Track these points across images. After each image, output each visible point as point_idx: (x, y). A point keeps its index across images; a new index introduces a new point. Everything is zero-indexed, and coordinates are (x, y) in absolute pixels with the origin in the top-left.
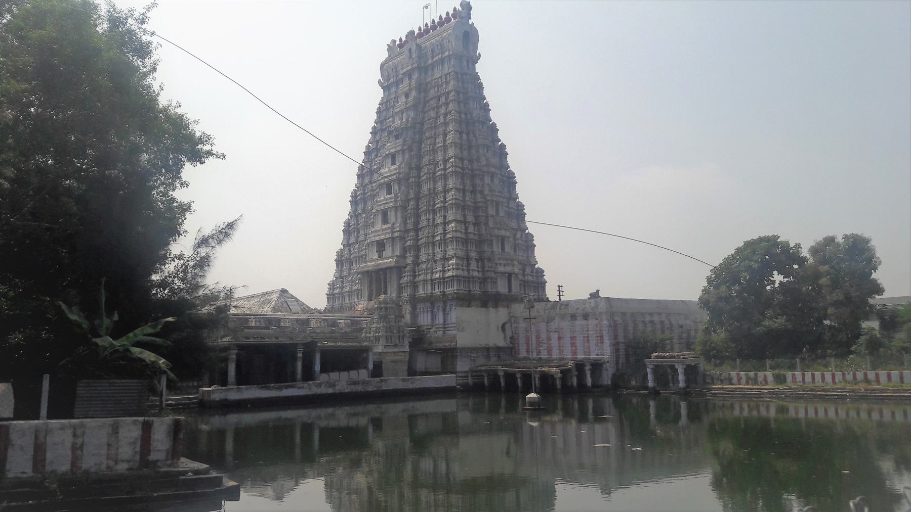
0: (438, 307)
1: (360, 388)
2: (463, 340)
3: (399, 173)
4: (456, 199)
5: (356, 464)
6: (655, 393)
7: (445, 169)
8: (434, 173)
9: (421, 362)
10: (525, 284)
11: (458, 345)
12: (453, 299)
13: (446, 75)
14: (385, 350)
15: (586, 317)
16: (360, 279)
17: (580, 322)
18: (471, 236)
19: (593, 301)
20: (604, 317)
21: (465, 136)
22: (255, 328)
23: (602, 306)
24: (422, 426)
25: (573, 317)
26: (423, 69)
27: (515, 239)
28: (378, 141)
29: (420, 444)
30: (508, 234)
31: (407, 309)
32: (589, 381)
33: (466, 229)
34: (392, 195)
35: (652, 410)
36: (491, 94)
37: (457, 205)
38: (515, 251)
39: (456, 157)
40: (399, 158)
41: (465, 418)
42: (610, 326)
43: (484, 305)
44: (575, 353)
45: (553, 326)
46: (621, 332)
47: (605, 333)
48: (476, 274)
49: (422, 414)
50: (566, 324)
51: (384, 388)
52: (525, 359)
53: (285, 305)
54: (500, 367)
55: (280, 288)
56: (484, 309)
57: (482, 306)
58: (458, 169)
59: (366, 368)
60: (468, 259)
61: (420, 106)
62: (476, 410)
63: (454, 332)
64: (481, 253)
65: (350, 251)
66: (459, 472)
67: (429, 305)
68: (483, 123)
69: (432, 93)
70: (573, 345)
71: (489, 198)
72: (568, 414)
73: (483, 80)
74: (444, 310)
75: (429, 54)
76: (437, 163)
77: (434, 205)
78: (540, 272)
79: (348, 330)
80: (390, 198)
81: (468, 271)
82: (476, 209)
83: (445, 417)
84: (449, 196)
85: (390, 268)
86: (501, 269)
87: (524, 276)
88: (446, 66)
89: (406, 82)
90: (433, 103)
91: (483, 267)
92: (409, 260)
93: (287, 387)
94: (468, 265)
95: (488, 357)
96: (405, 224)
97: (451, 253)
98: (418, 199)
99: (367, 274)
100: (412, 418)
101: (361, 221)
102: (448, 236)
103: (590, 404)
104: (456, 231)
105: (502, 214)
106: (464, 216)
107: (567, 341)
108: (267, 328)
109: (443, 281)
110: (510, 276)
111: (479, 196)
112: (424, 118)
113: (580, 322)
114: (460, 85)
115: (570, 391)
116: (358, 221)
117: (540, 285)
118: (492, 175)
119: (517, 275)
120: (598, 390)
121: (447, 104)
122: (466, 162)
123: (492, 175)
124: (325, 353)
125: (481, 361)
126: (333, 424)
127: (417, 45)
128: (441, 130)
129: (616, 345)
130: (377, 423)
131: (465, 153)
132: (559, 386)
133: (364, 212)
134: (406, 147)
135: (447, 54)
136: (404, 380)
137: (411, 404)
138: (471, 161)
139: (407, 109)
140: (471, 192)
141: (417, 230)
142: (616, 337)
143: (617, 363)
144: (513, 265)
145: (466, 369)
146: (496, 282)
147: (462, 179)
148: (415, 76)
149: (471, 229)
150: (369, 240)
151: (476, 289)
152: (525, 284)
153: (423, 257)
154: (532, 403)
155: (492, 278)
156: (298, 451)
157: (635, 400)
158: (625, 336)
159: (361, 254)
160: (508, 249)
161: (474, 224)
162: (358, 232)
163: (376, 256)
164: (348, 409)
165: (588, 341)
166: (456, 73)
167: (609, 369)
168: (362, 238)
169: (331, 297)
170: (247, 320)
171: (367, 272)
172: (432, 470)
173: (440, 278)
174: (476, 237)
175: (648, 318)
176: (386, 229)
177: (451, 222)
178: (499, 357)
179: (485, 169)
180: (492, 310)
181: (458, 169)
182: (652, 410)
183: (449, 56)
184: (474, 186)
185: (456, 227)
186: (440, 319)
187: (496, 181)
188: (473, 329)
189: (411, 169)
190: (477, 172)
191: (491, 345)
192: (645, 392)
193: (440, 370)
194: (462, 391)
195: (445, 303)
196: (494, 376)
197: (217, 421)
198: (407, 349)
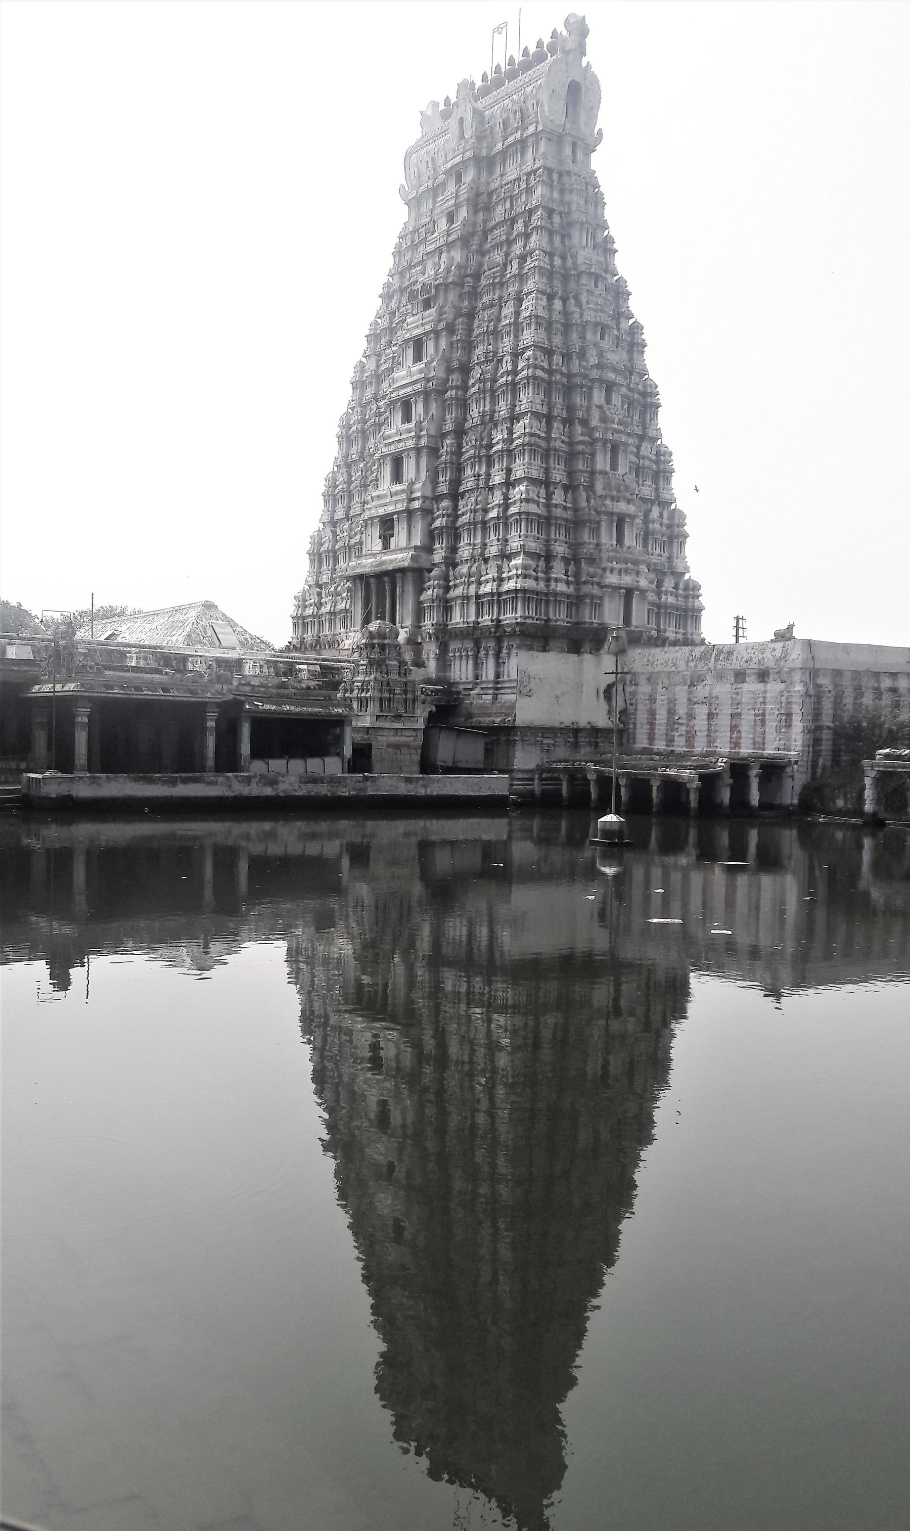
0: (487, 650)
1: (324, 790)
2: (528, 712)
3: (428, 380)
4: (532, 435)
5: (324, 923)
6: (875, 823)
7: (515, 372)
8: (494, 380)
9: (446, 748)
10: (658, 610)
11: (518, 723)
12: (513, 635)
13: (528, 174)
14: (378, 724)
15: (763, 676)
16: (349, 590)
17: (751, 686)
18: (558, 512)
19: (779, 645)
20: (797, 677)
21: (558, 304)
22: (135, 669)
23: (796, 656)
24: (443, 861)
25: (740, 676)
26: (486, 162)
27: (646, 521)
28: (393, 314)
29: (443, 894)
30: (632, 509)
31: (430, 650)
32: (755, 797)
33: (549, 496)
34: (414, 422)
35: (867, 856)
36: (619, 218)
37: (532, 448)
38: (645, 545)
39: (536, 346)
40: (429, 348)
41: (523, 851)
42: (807, 695)
43: (575, 648)
44: (736, 744)
45: (701, 691)
46: (827, 706)
47: (796, 709)
48: (562, 587)
49: (444, 843)
50: (723, 690)
51: (370, 792)
52: (645, 751)
53: (210, 632)
54: (591, 766)
55: (201, 598)
56: (573, 658)
57: (570, 651)
58: (539, 373)
59: (339, 754)
60: (548, 557)
61: (474, 239)
62: (544, 841)
63: (513, 697)
64: (575, 546)
65: (334, 533)
66: (513, 946)
67: (470, 645)
68: (597, 278)
69: (499, 213)
70: (734, 728)
71: (597, 435)
72: (707, 853)
73: (605, 187)
74: (497, 656)
75: (498, 130)
76: (500, 361)
77: (490, 446)
78: (692, 590)
79: (313, 684)
80: (409, 431)
81: (548, 580)
82: (571, 456)
83: (488, 850)
84: (519, 428)
85: (402, 570)
86: (612, 579)
87: (659, 594)
88: (529, 154)
89: (451, 188)
90: (500, 234)
91: (577, 575)
92: (438, 556)
93: (185, 781)
94: (548, 569)
95: (576, 745)
96: (434, 483)
97: (515, 544)
98: (460, 432)
99: (361, 578)
100: (425, 847)
101: (357, 475)
102: (513, 510)
103: (754, 837)
104: (527, 500)
105: (622, 469)
106: (547, 471)
107: (723, 722)
108: (158, 671)
109: (498, 599)
110: (629, 593)
111: (579, 429)
112: (481, 265)
113: (751, 686)
114: (556, 195)
115: (716, 813)
116: (350, 476)
117: (688, 613)
118: (609, 388)
119: (643, 592)
120: (773, 813)
121: (527, 236)
122: (557, 359)
123: (609, 388)
124: (261, 723)
125: (561, 752)
126: (275, 849)
127: (475, 111)
128: (512, 289)
129: (814, 734)
130: (360, 855)
131: (557, 340)
132: (694, 804)
133: (362, 458)
134: (442, 325)
135: (531, 129)
136: (408, 780)
137: (421, 823)
138: (567, 356)
139: (449, 245)
140: (565, 421)
141: (455, 496)
142: (817, 715)
143: (814, 765)
144: (638, 573)
145: (532, 766)
146: (601, 605)
147: (548, 393)
148: (469, 176)
149: (558, 497)
150: (367, 515)
151: (560, 617)
152: (658, 610)
153: (464, 552)
154: (608, 832)
155: (592, 597)
156: (208, 894)
157: (839, 835)
158: (835, 717)
159: (353, 541)
160: (629, 539)
161: (566, 488)
162: (351, 497)
163: (377, 545)
164: (301, 825)
165: (763, 722)
166: (550, 171)
167: (797, 775)
168: (356, 509)
169: (300, 622)
170: (123, 655)
171: (361, 577)
172: (464, 939)
173: (492, 594)
174: (569, 515)
175: (887, 683)
176: (397, 493)
177: (519, 481)
178: (596, 745)
179: (595, 374)
180: (587, 656)
181: (539, 373)
182: (867, 856)
183: (536, 134)
184: (570, 408)
185: (527, 491)
186: (488, 672)
187: (616, 399)
188: (547, 691)
189: (449, 370)
190: (578, 380)
191: (583, 723)
192: (859, 821)
193: (481, 766)
194: (517, 805)
195: (499, 640)
196: (576, 777)
197: (53, 834)
198: (421, 724)
